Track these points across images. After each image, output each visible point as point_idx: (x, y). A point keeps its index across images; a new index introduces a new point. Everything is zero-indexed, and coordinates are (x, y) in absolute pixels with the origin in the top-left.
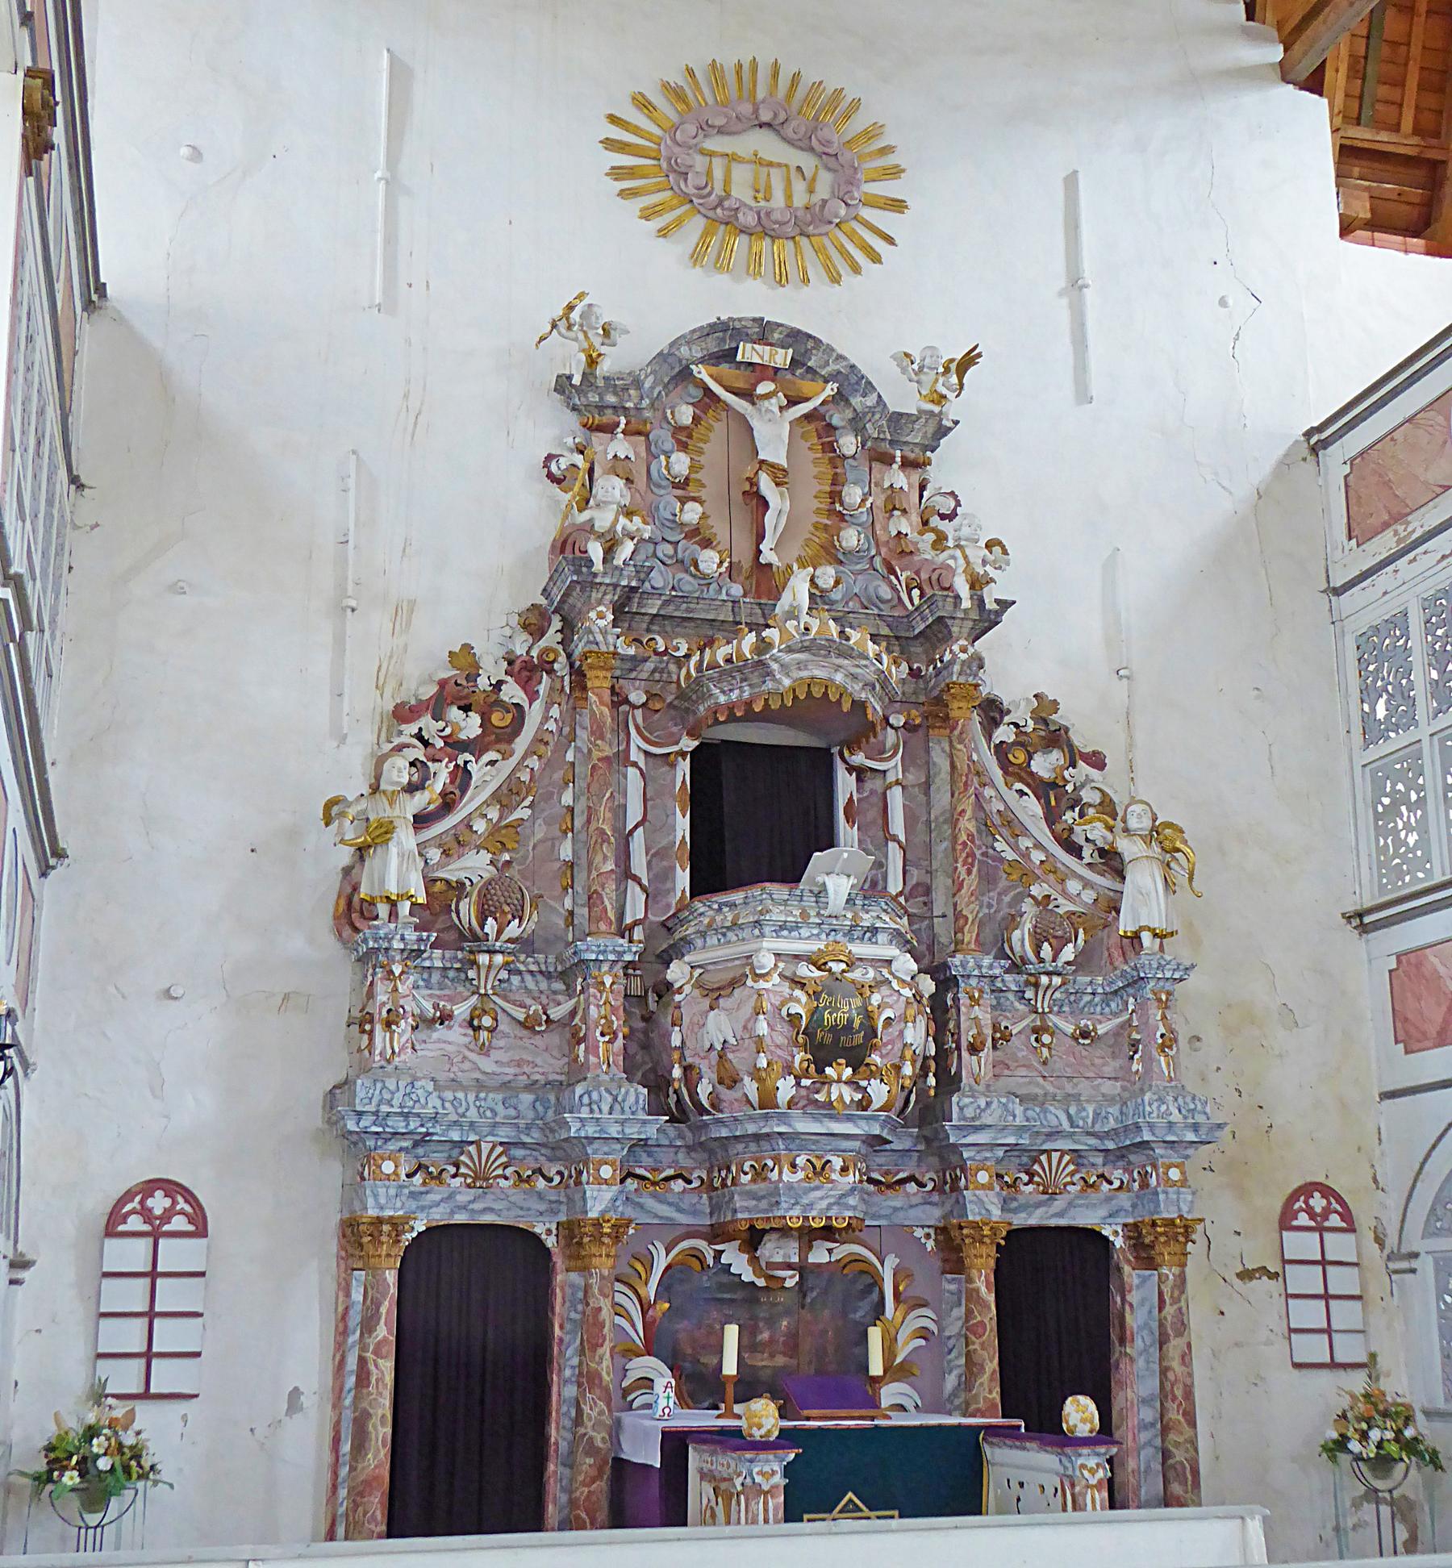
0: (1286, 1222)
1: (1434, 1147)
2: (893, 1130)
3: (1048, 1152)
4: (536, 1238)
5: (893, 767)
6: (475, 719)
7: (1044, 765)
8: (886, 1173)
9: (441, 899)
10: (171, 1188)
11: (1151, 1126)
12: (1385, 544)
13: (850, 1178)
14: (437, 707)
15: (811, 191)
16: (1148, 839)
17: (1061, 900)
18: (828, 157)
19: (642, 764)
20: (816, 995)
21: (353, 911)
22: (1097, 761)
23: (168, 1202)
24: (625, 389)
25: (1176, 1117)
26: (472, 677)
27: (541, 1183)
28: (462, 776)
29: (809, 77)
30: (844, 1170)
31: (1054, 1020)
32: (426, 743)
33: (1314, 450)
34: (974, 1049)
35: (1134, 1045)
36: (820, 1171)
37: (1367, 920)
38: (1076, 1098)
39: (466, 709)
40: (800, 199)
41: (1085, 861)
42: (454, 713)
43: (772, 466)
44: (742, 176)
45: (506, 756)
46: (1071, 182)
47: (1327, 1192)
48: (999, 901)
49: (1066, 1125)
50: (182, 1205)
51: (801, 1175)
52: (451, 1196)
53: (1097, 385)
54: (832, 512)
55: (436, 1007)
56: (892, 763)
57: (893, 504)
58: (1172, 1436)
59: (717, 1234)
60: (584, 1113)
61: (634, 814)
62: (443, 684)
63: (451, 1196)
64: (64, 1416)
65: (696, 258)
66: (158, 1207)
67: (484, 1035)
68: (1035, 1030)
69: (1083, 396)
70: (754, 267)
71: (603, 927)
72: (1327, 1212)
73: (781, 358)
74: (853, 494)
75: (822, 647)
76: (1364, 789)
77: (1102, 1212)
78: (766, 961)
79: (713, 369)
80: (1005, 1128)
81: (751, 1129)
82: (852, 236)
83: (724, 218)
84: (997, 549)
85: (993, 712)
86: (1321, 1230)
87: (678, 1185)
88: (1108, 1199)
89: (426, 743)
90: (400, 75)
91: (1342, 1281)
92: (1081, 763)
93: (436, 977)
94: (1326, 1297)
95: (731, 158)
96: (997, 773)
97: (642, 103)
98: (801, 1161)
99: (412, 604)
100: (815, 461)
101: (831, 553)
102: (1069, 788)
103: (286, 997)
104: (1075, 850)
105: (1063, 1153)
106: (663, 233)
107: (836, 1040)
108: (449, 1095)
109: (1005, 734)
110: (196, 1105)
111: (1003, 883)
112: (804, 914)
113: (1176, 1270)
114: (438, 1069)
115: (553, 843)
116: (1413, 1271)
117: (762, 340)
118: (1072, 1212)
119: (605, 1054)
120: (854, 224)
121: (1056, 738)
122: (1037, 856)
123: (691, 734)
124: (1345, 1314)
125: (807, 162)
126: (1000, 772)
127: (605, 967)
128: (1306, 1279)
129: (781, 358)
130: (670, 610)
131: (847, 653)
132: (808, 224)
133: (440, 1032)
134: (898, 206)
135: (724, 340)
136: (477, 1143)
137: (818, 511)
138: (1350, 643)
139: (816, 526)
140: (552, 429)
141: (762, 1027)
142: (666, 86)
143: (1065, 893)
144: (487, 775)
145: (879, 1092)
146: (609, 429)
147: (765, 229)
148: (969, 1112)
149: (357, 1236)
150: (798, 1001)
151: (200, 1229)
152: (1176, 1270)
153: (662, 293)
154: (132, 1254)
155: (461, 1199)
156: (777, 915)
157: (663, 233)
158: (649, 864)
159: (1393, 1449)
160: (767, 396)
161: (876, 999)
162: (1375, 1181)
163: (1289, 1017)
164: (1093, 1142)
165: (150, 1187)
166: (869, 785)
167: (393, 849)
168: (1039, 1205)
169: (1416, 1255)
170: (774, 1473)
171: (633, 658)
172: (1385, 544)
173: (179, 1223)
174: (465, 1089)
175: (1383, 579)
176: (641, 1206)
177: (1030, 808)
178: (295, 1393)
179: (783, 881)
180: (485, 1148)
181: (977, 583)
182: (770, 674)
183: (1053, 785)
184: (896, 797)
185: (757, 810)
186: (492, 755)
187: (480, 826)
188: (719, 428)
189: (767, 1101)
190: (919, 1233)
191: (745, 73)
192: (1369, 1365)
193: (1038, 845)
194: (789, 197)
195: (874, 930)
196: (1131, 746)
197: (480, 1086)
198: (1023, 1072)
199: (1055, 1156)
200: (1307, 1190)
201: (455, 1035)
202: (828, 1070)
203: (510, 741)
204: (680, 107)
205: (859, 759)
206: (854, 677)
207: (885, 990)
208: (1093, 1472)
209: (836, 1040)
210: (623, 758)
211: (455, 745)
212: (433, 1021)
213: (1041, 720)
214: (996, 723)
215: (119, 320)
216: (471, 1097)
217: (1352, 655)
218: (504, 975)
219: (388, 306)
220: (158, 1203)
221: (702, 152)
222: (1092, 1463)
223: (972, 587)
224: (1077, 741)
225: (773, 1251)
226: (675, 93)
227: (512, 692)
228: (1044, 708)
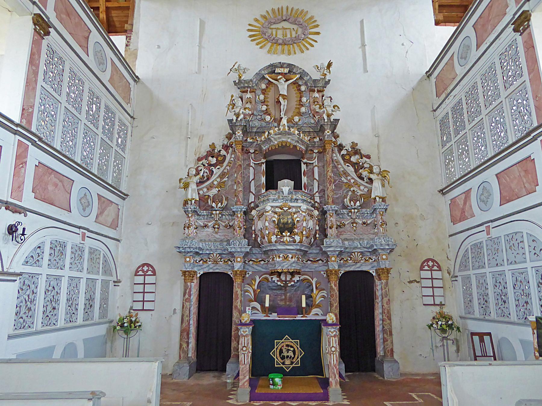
0: (422, 269)
1: (459, 248)
2: (309, 249)
3: (354, 252)
4: (229, 275)
6: (215, 159)
7: (354, 159)
8: (314, 258)
10: (148, 265)
11: (376, 245)
12: (443, 96)
13: (294, 260)
14: (206, 157)
15: (296, 33)
16: (378, 175)
17: (358, 191)
18: (300, 25)
19: (253, 166)
20: (280, 215)
22: (368, 157)
23: (147, 268)
24: (249, 82)
25: (383, 242)
26: (214, 150)
27: (230, 263)
28: (212, 172)
29: (296, 8)
30: (292, 257)
31: (357, 220)
32: (204, 165)
33: (428, 77)
34: (331, 228)
35: (375, 225)
36: (286, 258)
37: (444, 191)
38: (363, 239)
39: (213, 157)
40: (294, 36)
41: (366, 181)
42: (210, 158)
43: (282, 95)
44: (280, 33)
45: (222, 167)
46: (362, 22)
47: (433, 261)
48: (343, 192)
49: (359, 246)
50: (150, 269)
51: (281, 259)
52: (209, 266)
53: (369, 68)
54: (300, 104)
55: (204, 224)
56: (314, 161)
58: (384, 322)
59: (272, 274)
60: (232, 246)
61: (252, 177)
62: (207, 152)
63: (209, 266)
64: (121, 314)
66: (146, 269)
67: (216, 229)
68: (352, 223)
69: (366, 71)
70: (283, 52)
71: (239, 203)
72: (433, 266)
73: (286, 71)
74: (304, 99)
75: (284, 133)
76: (443, 158)
77: (370, 267)
78: (268, 208)
79: (269, 75)
80: (337, 247)
81: (269, 248)
82: (307, 42)
83: (275, 42)
84: (336, 108)
85: (341, 147)
86: (431, 270)
87: (262, 262)
88: (371, 264)
89: (204, 165)
90: (202, 24)
91: (436, 283)
92: (364, 158)
93: (206, 217)
94: (433, 287)
95: (277, 29)
96: (342, 162)
97: (256, 20)
98: (281, 256)
99: (203, 136)
100: (296, 93)
101: (300, 114)
102: (361, 164)
103: (173, 223)
104: (362, 179)
105: (358, 252)
106: (261, 48)
107: (284, 226)
108: (207, 243)
109: (344, 152)
111: (344, 188)
112: (279, 197)
113: (385, 281)
115: (233, 185)
116: (457, 281)
117: (282, 67)
118: (362, 267)
119: (240, 232)
120: (307, 39)
121: (356, 152)
122: (352, 181)
123: (264, 158)
124: (438, 292)
125: (295, 27)
126: (342, 161)
127: (239, 212)
128: (429, 283)
129: (286, 71)
130: (259, 130)
131: (290, 134)
132: (295, 41)
133: (206, 229)
134: (318, 33)
135: (272, 69)
136: (213, 254)
137: (296, 105)
138: (438, 122)
139: (296, 108)
141: (267, 224)
142: (262, 16)
143: (360, 190)
144: (217, 171)
145: (297, 238)
146: (247, 92)
147: (284, 43)
148: (328, 243)
149: (187, 275)
150: (275, 217)
151: (154, 274)
152: (385, 281)
153: (257, 59)
154: (140, 279)
155: (211, 266)
156: (272, 197)
157: (261, 48)
158: (255, 189)
159: (444, 327)
160: (280, 79)
161: (295, 216)
162: (448, 258)
163: (422, 217)
164: (366, 250)
165: (143, 265)
166: (309, 167)
167: (190, 189)
168: (353, 265)
169: (457, 277)
170: (246, 331)
171: (251, 142)
172: (443, 96)
173: (150, 273)
174: (211, 242)
175: (443, 106)
176: (253, 267)
177: (351, 170)
178: (175, 309)
179: (273, 189)
180: (215, 255)
181: (329, 116)
182: (271, 141)
183: (356, 163)
184: (316, 170)
185: (282, 168)
186: (218, 167)
187: (215, 183)
188: (273, 89)
189: (270, 242)
190: (322, 273)
191: (280, 10)
192: (441, 305)
193: (353, 178)
194: (291, 35)
195: (297, 200)
196: (379, 153)
197: (215, 241)
198: (349, 233)
199: (356, 253)
200: (428, 260)
201: (210, 230)
202: (284, 234)
203: (223, 163)
204: (265, 19)
205: (305, 161)
206: (293, 140)
207: (298, 214)
208: (332, 333)
209: (284, 226)
210: (249, 165)
212: (203, 227)
213: (353, 148)
214: (342, 150)
215: (143, 83)
216: (212, 243)
217: (439, 126)
218: (220, 216)
219: (199, 72)
220: (145, 268)
221: (271, 29)
222: (332, 330)
223: (328, 116)
224: (363, 152)
225: (283, 277)
226: (264, 17)
227: (223, 152)
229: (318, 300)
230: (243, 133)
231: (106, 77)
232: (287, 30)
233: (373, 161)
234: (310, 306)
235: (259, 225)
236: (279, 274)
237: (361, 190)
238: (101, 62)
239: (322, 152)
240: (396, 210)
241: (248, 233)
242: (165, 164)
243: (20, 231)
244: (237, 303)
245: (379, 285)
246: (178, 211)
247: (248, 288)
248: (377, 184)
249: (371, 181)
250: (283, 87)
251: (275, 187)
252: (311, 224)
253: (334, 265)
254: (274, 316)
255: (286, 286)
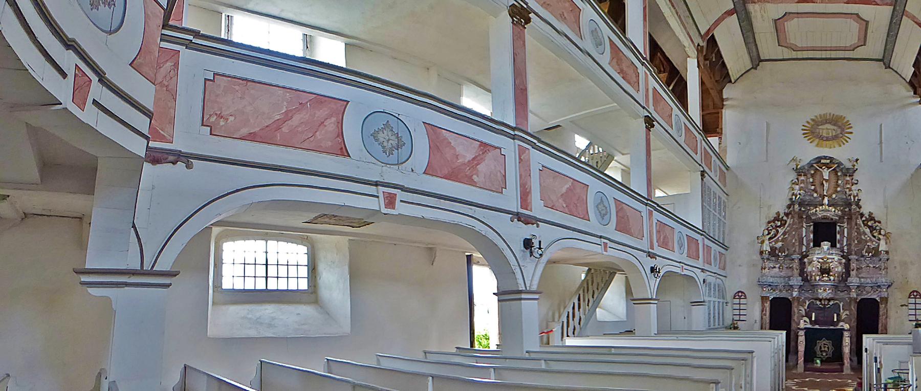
5: (845, 225)
7: (870, 224)
9: (773, 249)
18: (839, 127)
21: (761, 253)
22: (880, 222)
28: (778, 231)
57: (847, 182)
65: (817, 145)
66: (740, 295)
73: (828, 161)
74: (840, 182)
83: (821, 138)
85: (862, 215)
97: (808, 122)
101: (836, 192)
110: (744, 281)
114: (774, 273)
119: (796, 272)
121: (871, 218)
125: (835, 128)
128: (913, 306)
132: (835, 138)
135: (818, 160)
140: (793, 176)
145: (832, 278)
147: (828, 139)
149: (764, 299)
153: (809, 152)
154: (737, 301)
163: (912, 263)
177: (867, 230)
185: (824, 232)
200: (914, 291)
201: (777, 270)
211: (777, 226)
219: (767, 161)
226: (813, 120)
227: (785, 218)
228: (870, 214)
229: (843, 317)
230: (799, 208)
231: (681, 140)
232: (827, 130)
233: (883, 226)
234: (839, 320)
235: (809, 269)
236: (820, 300)
237: (873, 245)
238: (599, 44)
239: (850, 219)
240: (895, 258)
241: (802, 273)
242: (750, 226)
243: (536, 245)
244: (795, 318)
245: (882, 306)
246: (757, 257)
247: (801, 308)
248: (882, 242)
249: (879, 239)
250: (826, 174)
251: (819, 246)
252: (840, 269)
253: (853, 295)
254: (817, 327)
255: (825, 308)
